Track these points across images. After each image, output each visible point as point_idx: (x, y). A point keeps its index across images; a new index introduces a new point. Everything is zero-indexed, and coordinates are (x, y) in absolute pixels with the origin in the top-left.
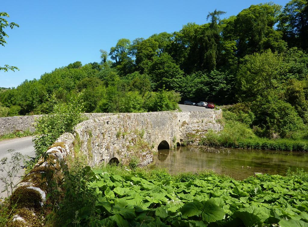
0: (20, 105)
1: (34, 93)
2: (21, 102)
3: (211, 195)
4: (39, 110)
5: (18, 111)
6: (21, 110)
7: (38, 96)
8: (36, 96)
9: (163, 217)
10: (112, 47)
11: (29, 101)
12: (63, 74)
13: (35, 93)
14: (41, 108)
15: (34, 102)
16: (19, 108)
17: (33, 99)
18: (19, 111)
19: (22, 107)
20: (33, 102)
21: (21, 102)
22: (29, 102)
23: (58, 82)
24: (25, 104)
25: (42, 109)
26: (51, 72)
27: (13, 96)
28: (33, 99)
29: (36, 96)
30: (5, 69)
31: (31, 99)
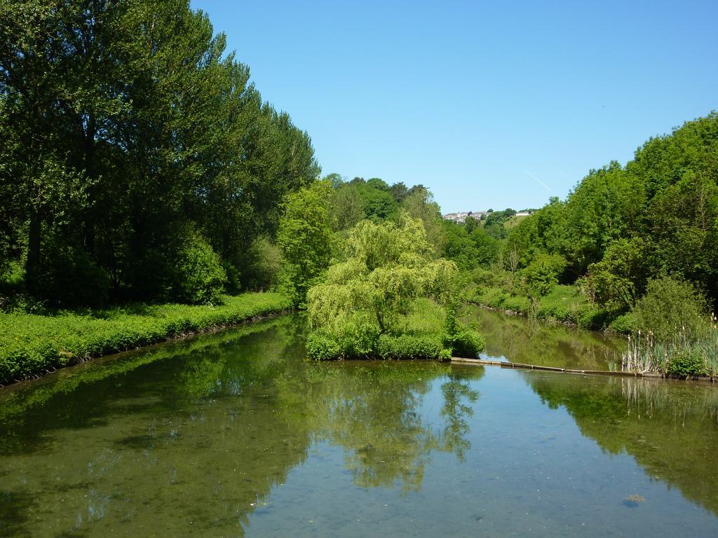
0: (563, 251)
1: (604, 208)
2: (567, 243)
3: (156, 322)
4: (606, 268)
5: (555, 270)
6: (568, 268)
7: (618, 218)
8: (613, 217)
9: (173, 307)
10: (635, 152)
11: (588, 235)
12: (708, 129)
13: (609, 205)
14: (614, 258)
15: (606, 238)
16: (561, 261)
17: (602, 228)
18: (561, 270)
19: (569, 259)
20: (600, 241)
21: (567, 241)
22: (586, 241)
23: (688, 157)
24: (577, 247)
25: (616, 263)
26: (549, 203)
27: (548, 224)
28: (602, 228)
29: (613, 217)
30: (152, 500)
31: (594, 228)
